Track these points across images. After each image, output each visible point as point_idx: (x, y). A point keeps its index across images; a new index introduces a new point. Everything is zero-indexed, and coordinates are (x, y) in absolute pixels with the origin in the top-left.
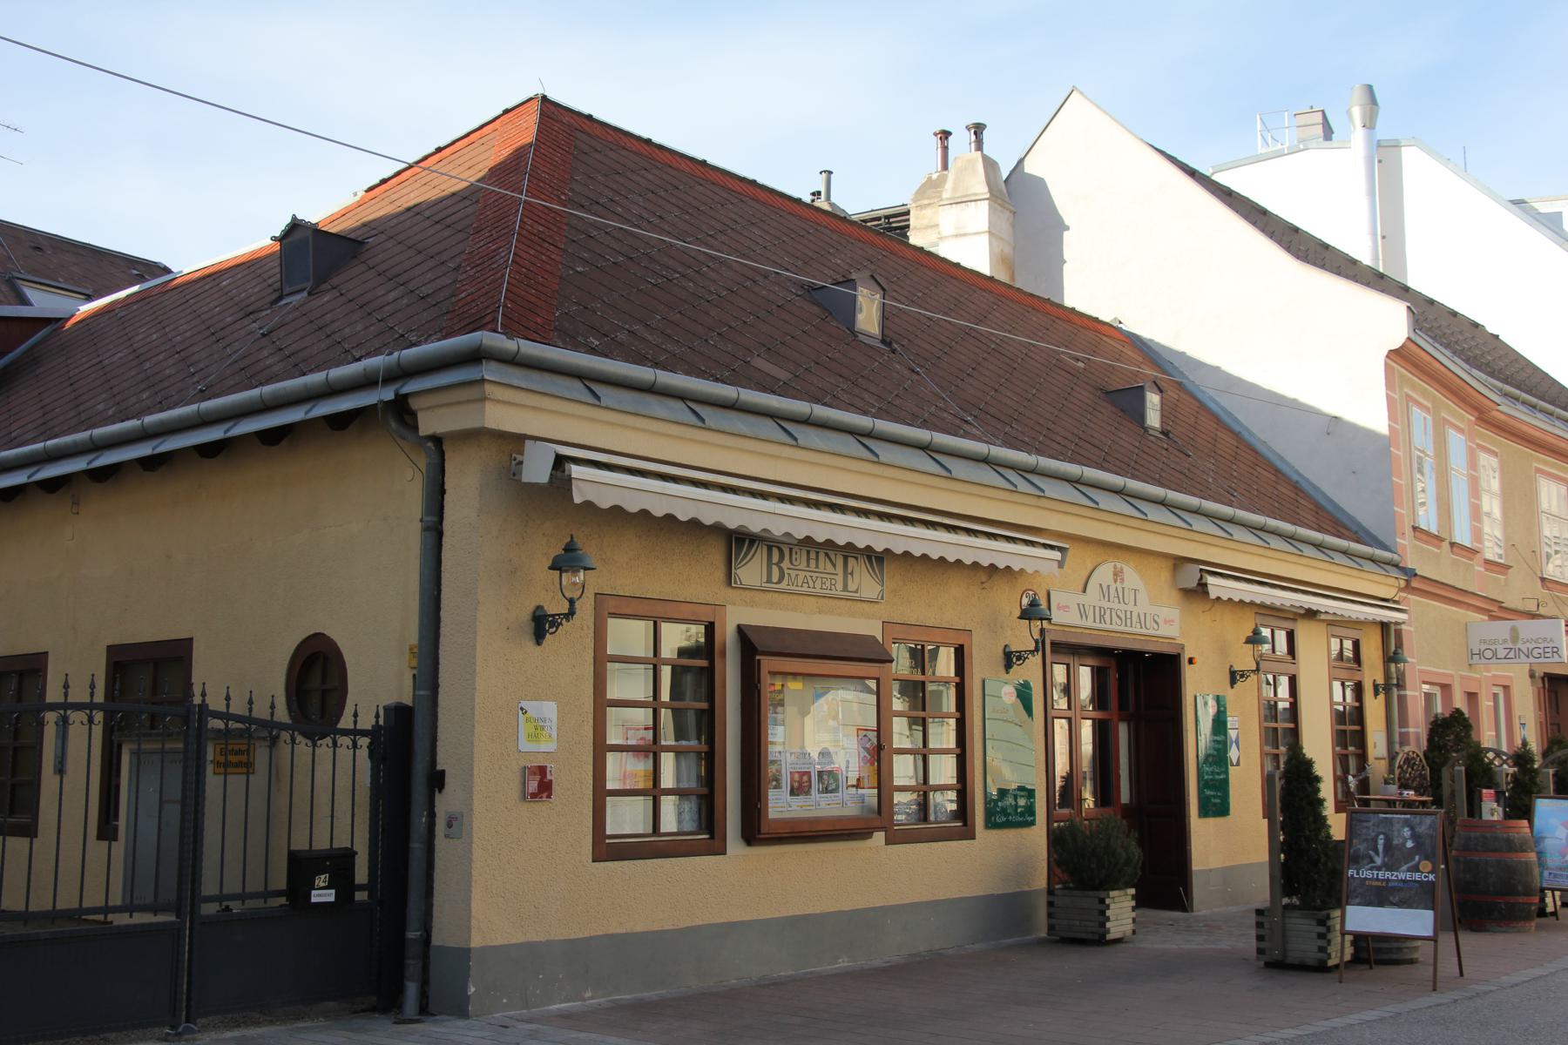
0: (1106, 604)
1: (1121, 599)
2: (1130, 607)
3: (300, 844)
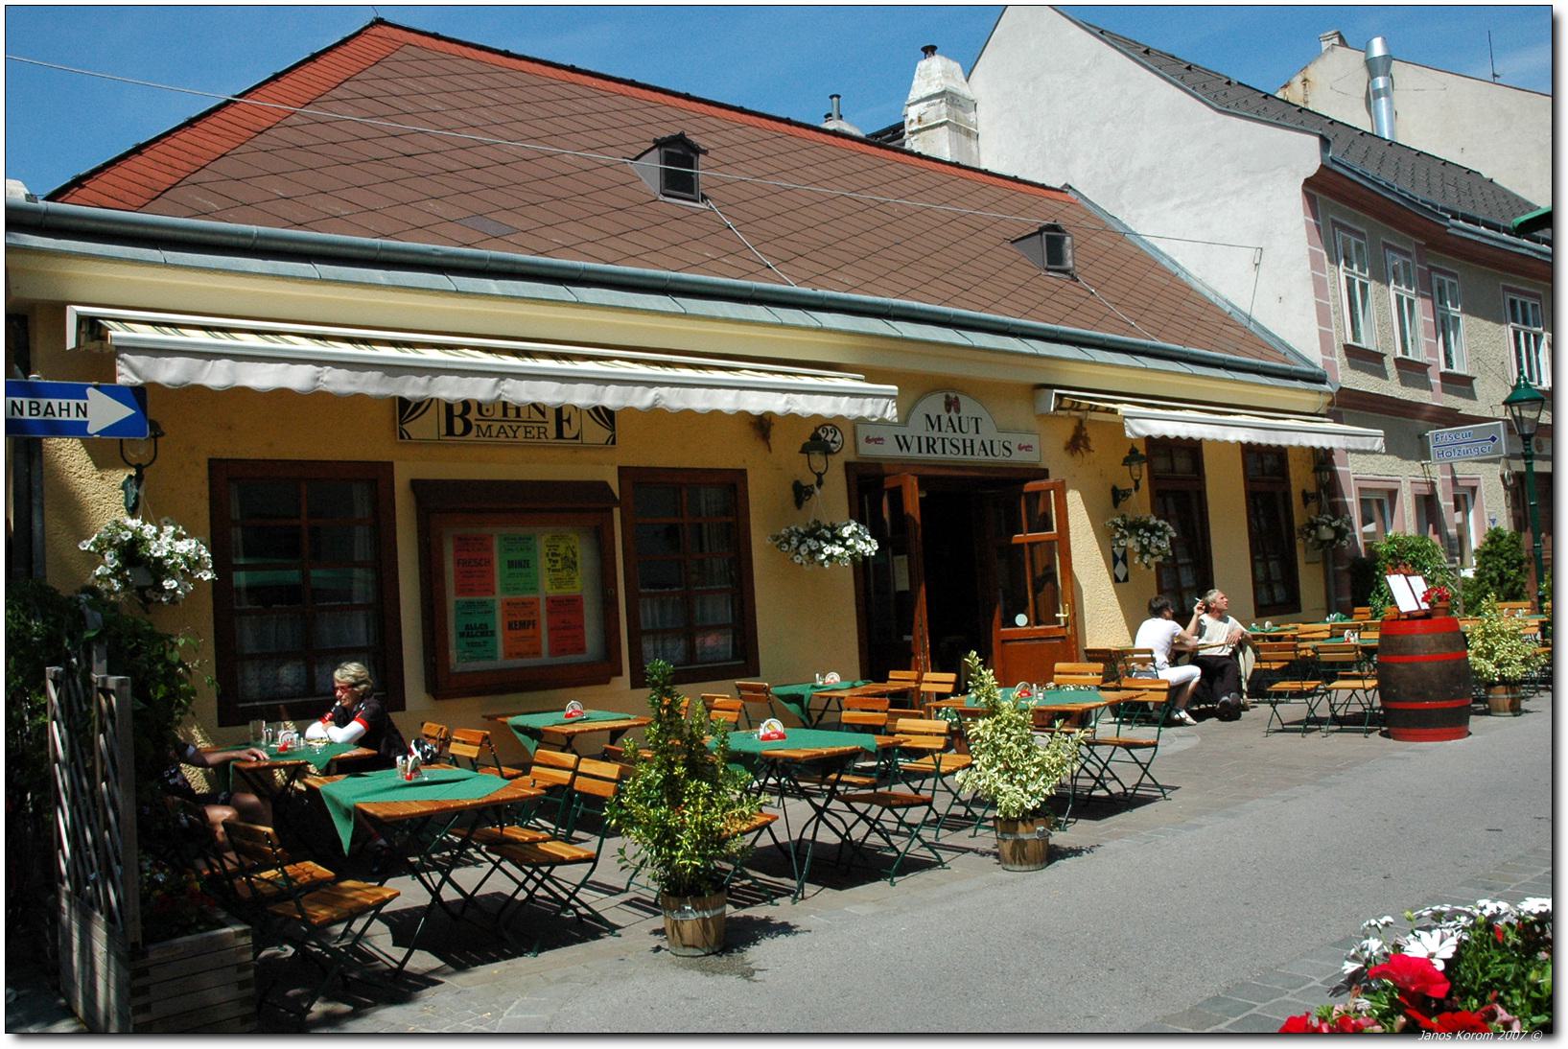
0: (935, 434)
2: (971, 434)
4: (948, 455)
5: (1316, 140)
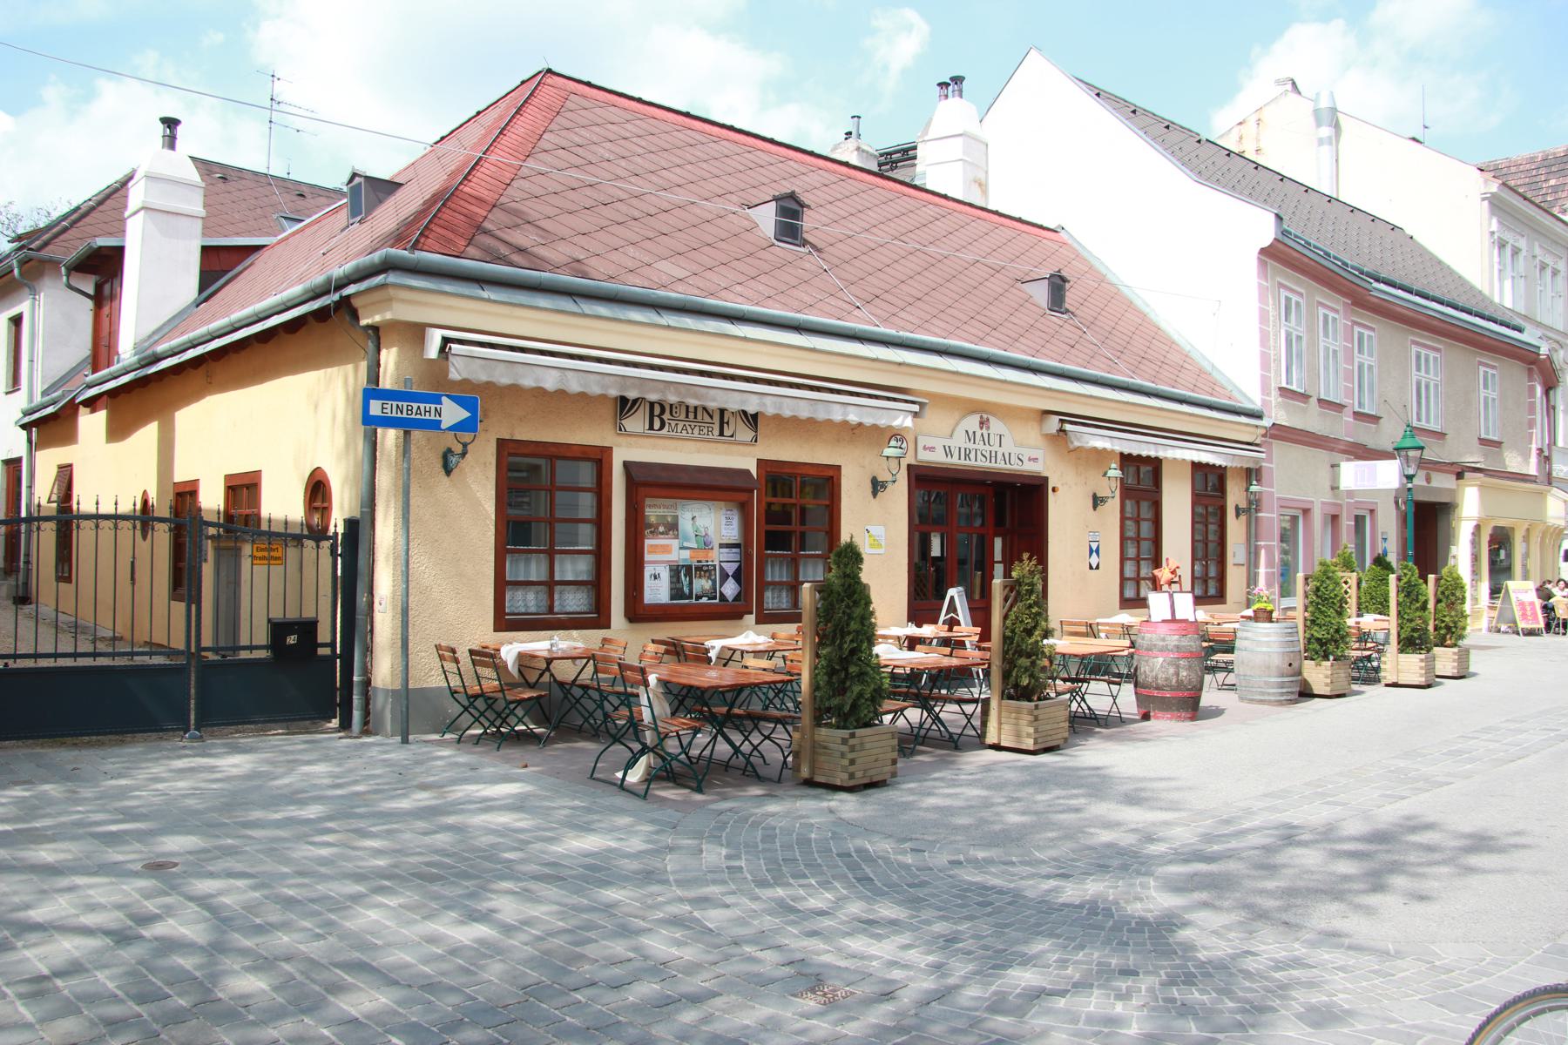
0: (971, 446)
1: (986, 441)
2: (996, 448)
3: (277, 614)
4: (979, 463)
5: (1272, 218)
